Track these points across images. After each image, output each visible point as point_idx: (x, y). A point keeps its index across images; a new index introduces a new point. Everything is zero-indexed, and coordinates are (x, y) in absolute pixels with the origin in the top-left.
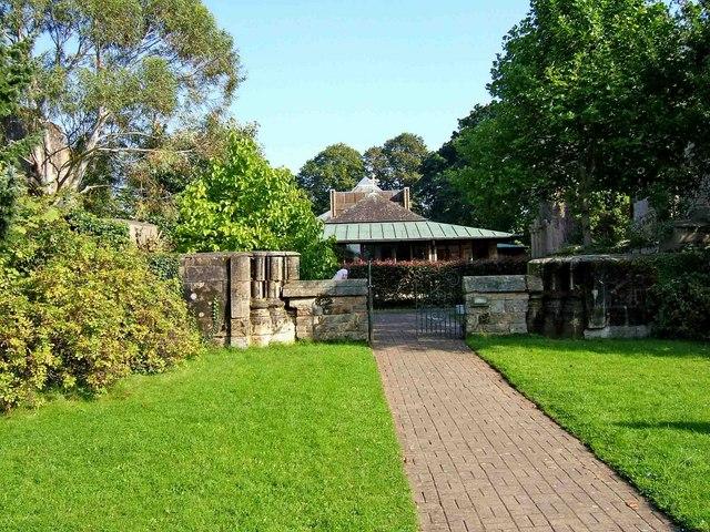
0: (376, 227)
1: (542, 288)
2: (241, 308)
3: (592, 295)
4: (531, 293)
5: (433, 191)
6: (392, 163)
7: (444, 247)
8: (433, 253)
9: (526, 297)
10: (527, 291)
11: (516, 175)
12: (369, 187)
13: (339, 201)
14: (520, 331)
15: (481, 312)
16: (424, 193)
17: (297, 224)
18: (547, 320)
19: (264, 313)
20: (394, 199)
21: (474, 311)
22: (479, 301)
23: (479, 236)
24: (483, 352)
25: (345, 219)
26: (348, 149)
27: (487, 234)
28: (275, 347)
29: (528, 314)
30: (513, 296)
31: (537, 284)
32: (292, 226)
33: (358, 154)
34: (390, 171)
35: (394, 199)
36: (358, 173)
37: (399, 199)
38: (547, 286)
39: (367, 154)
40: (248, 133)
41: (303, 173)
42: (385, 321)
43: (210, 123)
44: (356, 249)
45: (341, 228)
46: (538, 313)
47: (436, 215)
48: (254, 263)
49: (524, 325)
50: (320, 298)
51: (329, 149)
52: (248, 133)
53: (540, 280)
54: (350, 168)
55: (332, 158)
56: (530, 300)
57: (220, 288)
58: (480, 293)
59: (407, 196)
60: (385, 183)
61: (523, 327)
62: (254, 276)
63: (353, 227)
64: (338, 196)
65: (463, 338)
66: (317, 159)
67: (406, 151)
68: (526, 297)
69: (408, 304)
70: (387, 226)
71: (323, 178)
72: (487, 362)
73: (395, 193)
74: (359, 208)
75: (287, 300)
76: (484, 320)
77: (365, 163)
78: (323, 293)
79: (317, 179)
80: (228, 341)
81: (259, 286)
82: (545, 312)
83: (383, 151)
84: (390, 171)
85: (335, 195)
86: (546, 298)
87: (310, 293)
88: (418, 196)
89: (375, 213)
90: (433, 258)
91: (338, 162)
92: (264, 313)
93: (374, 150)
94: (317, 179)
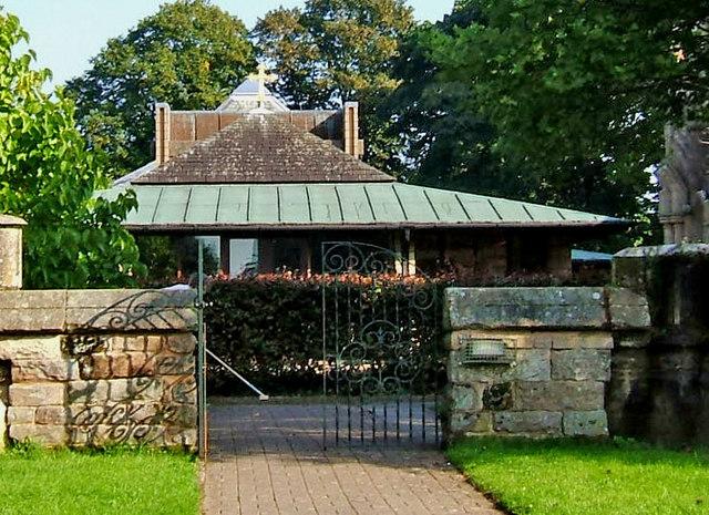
1: (645, 320)
4: (620, 333)
5: (423, 123)
6: (326, 49)
7: (433, 243)
8: (406, 256)
9: (607, 341)
10: (607, 328)
11: (601, 45)
12: (256, 100)
13: (181, 133)
14: (590, 431)
15: (490, 378)
16: (401, 127)
17: (38, 161)
18: (658, 401)
20: (321, 131)
21: (471, 375)
22: (484, 348)
23: (524, 220)
24: (484, 472)
25: (189, 173)
26: (215, 13)
27: (545, 215)
29: (610, 388)
30: (574, 340)
31: (635, 310)
32: (25, 167)
33: (237, 25)
34: (321, 71)
35: (321, 131)
36: (231, 70)
37: (333, 131)
38: (660, 317)
39: (264, 27)
41: (99, 71)
42: (261, 412)
43: (251, 279)
45: (175, 194)
46: (635, 384)
47: (435, 172)
49: (600, 415)
51: (166, 11)
53: (643, 299)
54: (218, 62)
55: (174, 35)
56: (617, 350)
58: (489, 330)
59: (351, 126)
60: (295, 87)
61: (595, 418)
65: (442, 446)
66: (134, 35)
67: (361, 20)
68: (607, 341)
69: (342, 386)
70: (292, 192)
71: (149, 84)
72: (489, 496)
73: (320, 116)
74: (222, 147)
76: (497, 398)
77: (256, 50)
78: (82, 320)
79: (133, 87)
82: (654, 381)
83: (303, 20)
84: (321, 71)
85: (166, 118)
86: (657, 346)
87: (46, 321)
88: (388, 134)
89: (263, 157)
90: (407, 270)
91: (187, 46)
93: (279, 16)
94: (133, 87)
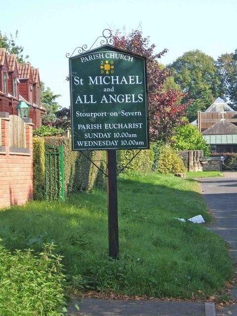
0: (224, 137)
2: (191, 163)
3: (194, 215)
19: (196, 164)
26: (203, 56)
28: (198, 172)
39: (220, 60)
40: (137, 37)
44: (215, 147)
48: (194, 153)
50: (209, 161)
52: (137, 37)
57: (187, 158)
62: (194, 156)
63: (213, 137)
64: (202, 114)
75: (201, 162)
80: (188, 170)
81: (195, 158)
92: (196, 164)
